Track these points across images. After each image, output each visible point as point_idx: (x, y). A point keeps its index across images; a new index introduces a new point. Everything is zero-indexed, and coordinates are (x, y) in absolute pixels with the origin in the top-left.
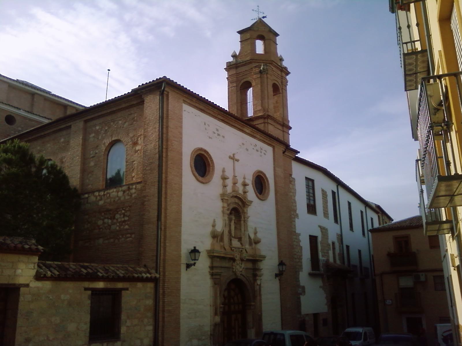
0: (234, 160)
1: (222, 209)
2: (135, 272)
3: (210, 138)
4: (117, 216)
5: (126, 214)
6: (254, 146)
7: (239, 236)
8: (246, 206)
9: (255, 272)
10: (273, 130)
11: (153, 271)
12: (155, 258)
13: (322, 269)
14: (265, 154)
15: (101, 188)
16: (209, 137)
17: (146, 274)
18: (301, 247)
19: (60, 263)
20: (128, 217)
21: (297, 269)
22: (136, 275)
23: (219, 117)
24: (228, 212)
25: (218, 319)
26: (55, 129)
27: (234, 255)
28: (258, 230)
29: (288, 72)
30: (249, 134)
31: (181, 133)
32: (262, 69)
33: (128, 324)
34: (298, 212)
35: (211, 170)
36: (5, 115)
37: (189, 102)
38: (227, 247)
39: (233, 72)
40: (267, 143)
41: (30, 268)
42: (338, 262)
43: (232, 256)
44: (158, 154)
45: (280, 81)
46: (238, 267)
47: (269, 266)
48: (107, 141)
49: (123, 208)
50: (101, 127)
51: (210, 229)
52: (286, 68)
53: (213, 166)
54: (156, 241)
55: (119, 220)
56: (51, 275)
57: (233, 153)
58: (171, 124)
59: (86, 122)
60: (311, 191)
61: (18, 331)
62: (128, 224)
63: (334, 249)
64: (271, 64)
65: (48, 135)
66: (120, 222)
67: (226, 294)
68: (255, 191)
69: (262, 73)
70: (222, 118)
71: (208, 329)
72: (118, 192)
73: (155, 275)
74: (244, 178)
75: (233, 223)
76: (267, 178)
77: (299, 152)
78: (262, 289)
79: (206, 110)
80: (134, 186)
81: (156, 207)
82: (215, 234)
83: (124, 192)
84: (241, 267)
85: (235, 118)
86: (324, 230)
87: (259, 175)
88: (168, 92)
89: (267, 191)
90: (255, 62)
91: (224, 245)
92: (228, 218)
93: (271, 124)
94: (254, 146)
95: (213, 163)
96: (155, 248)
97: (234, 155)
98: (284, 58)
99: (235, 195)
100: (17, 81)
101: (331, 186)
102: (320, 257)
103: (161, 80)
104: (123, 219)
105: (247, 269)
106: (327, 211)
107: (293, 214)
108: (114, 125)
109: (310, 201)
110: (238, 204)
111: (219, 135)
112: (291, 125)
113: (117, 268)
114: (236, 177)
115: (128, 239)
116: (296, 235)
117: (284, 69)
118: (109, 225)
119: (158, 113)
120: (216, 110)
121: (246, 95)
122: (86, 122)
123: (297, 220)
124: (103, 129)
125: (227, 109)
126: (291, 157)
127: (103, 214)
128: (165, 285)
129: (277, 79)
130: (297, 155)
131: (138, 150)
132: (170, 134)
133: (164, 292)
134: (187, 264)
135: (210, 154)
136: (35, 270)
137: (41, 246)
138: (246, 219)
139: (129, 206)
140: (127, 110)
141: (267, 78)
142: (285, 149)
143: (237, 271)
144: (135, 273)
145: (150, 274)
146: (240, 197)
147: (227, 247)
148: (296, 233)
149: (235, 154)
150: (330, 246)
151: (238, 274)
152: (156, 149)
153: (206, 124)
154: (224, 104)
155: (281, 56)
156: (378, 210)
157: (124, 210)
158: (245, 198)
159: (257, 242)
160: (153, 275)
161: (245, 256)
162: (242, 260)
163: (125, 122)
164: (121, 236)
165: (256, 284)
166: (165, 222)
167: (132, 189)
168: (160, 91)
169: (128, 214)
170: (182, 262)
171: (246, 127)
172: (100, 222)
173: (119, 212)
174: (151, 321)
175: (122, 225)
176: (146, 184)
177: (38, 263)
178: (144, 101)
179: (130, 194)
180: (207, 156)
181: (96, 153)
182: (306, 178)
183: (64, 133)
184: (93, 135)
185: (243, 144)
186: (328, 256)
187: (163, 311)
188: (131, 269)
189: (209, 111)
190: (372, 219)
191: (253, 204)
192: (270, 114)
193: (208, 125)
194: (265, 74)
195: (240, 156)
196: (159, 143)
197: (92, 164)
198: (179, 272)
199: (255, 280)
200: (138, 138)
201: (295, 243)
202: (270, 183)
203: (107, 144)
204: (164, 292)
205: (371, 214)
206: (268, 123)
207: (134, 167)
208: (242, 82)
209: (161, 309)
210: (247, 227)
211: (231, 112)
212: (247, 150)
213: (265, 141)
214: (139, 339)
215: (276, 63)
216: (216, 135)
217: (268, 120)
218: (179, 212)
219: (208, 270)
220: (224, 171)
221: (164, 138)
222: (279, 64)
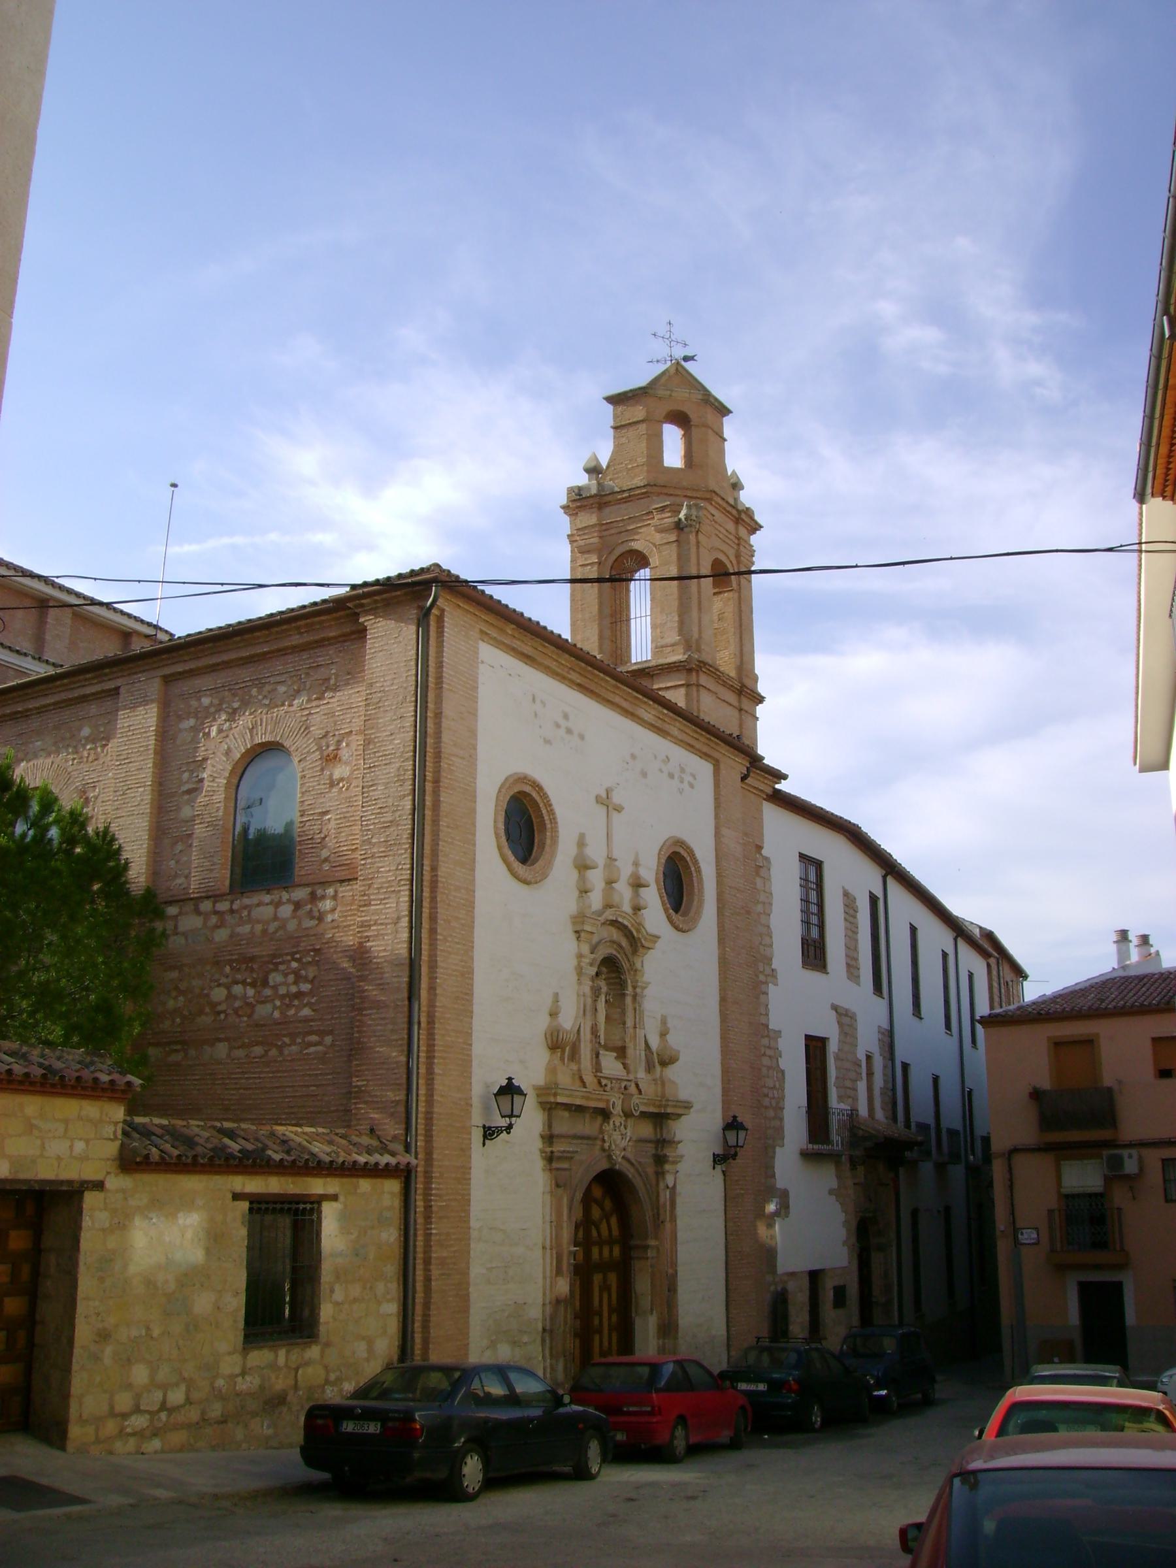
1: (574, 962)
4: (275, 978)
5: (303, 972)
7: (619, 1044)
9: (661, 1151)
10: (715, 709)
11: (400, 1148)
12: (402, 1109)
13: (835, 1137)
14: (692, 786)
18: (783, 1072)
20: (312, 982)
21: (772, 1137)
23: (574, 676)
24: (593, 971)
25: (563, 1286)
26: (63, 696)
27: (608, 1101)
28: (671, 1023)
29: (756, 523)
30: (652, 725)
31: (473, 733)
32: (682, 515)
33: (338, 1295)
34: (775, 964)
35: (548, 841)
38: (589, 1079)
39: (589, 519)
41: (106, 1136)
42: (880, 1115)
43: (601, 1105)
45: (731, 553)
46: (616, 1136)
47: (696, 1135)
52: (748, 512)
53: (555, 830)
55: (282, 990)
56: (162, 1158)
58: (450, 708)
59: (168, 680)
60: (813, 896)
61: (81, 1309)
62: (309, 1004)
63: (870, 1074)
64: (709, 500)
66: (283, 997)
68: (663, 904)
69: (682, 529)
71: (535, 1313)
72: (278, 904)
73: (404, 1159)
74: (636, 864)
75: (601, 1005)
76: (696, 862)
77: (785, 777)
78: (679, 1200)
79: (539, 659)
80: (330, 891)
83: (298, 905)
84: (623, 1136)
85: (596, 669)
86: (845, 1018)
87: (675, 853)
88: (443, 611)
90: (659, 494)
91: (579, 1070)
92: (592, 988)
95: (554, 820)
96: (404, 1081)
97: (608, 791)
99: (611, 918)
101: (868, 878)
102: (834, 1101)
104: (294, 989)
106: (856, 960)
108: (260, 697)
109: (809, 929)
110: (620, 946)
112: (762, 688)
115: (312, 1049)
116: (768, 1036)
117: (743, 516)
118: (247, 1004)
119: (414, 672)
120: (567, 656)
125: (566, 635)
126: (762, 791)
127: (228, 969)
128: (431, 1189)
129: (724, 547)
130: (777, 786)
131: (342, 779)
132: (446, 737)
133: (428, 1208)
138: (638, 990)
139: (314, 950)
143: (613, 1147)
145: (393, 1154)
146: (626, 923)
147: (589, 1079)
150: (860, 1066)
151: (618, 1155)
152: (404, 781)
153: (538, 701)
155: (734, 472)
156: (989, 946)
157: (298, 960)
158: (640, 925)
163: (298, 691)
164: (287, 1040)
165: (662, 1185)
166: (432, 1005)
167: (323, 897)
168: (421, 608)
172: (219, 994)
173: (282, 967)
174: (394, 1288)
175: (289, 1006)
182: (803, 857)
183: (93, 709)
184: (192, 722)
185: (633, 757)
186: (855, 1099)
187: (427, 1262)
189: (547, 662)
190: (971, 976)
191: (659, 944)
193: (542, 702)
196: (415, 765)
198: (465, 1151)
199: (660, 1174)
200: (339, 742)
201: (766, 1061)
203: (239, 756)
204: (428, 1208)
205: (971, 962)
206: (698, 685)
207: (325, 832)
208: (617, 552)
209: (420, 1255)
210: (642, 1012)
211: (579, 646)
212: (644, 774)
213: (692, 746)
214: (363, 1338)
216: (562, 732)
218: (467, 974)
219: (539, 1144)
220: (581, 843)
221: (428, 749)
222: (732, 502)
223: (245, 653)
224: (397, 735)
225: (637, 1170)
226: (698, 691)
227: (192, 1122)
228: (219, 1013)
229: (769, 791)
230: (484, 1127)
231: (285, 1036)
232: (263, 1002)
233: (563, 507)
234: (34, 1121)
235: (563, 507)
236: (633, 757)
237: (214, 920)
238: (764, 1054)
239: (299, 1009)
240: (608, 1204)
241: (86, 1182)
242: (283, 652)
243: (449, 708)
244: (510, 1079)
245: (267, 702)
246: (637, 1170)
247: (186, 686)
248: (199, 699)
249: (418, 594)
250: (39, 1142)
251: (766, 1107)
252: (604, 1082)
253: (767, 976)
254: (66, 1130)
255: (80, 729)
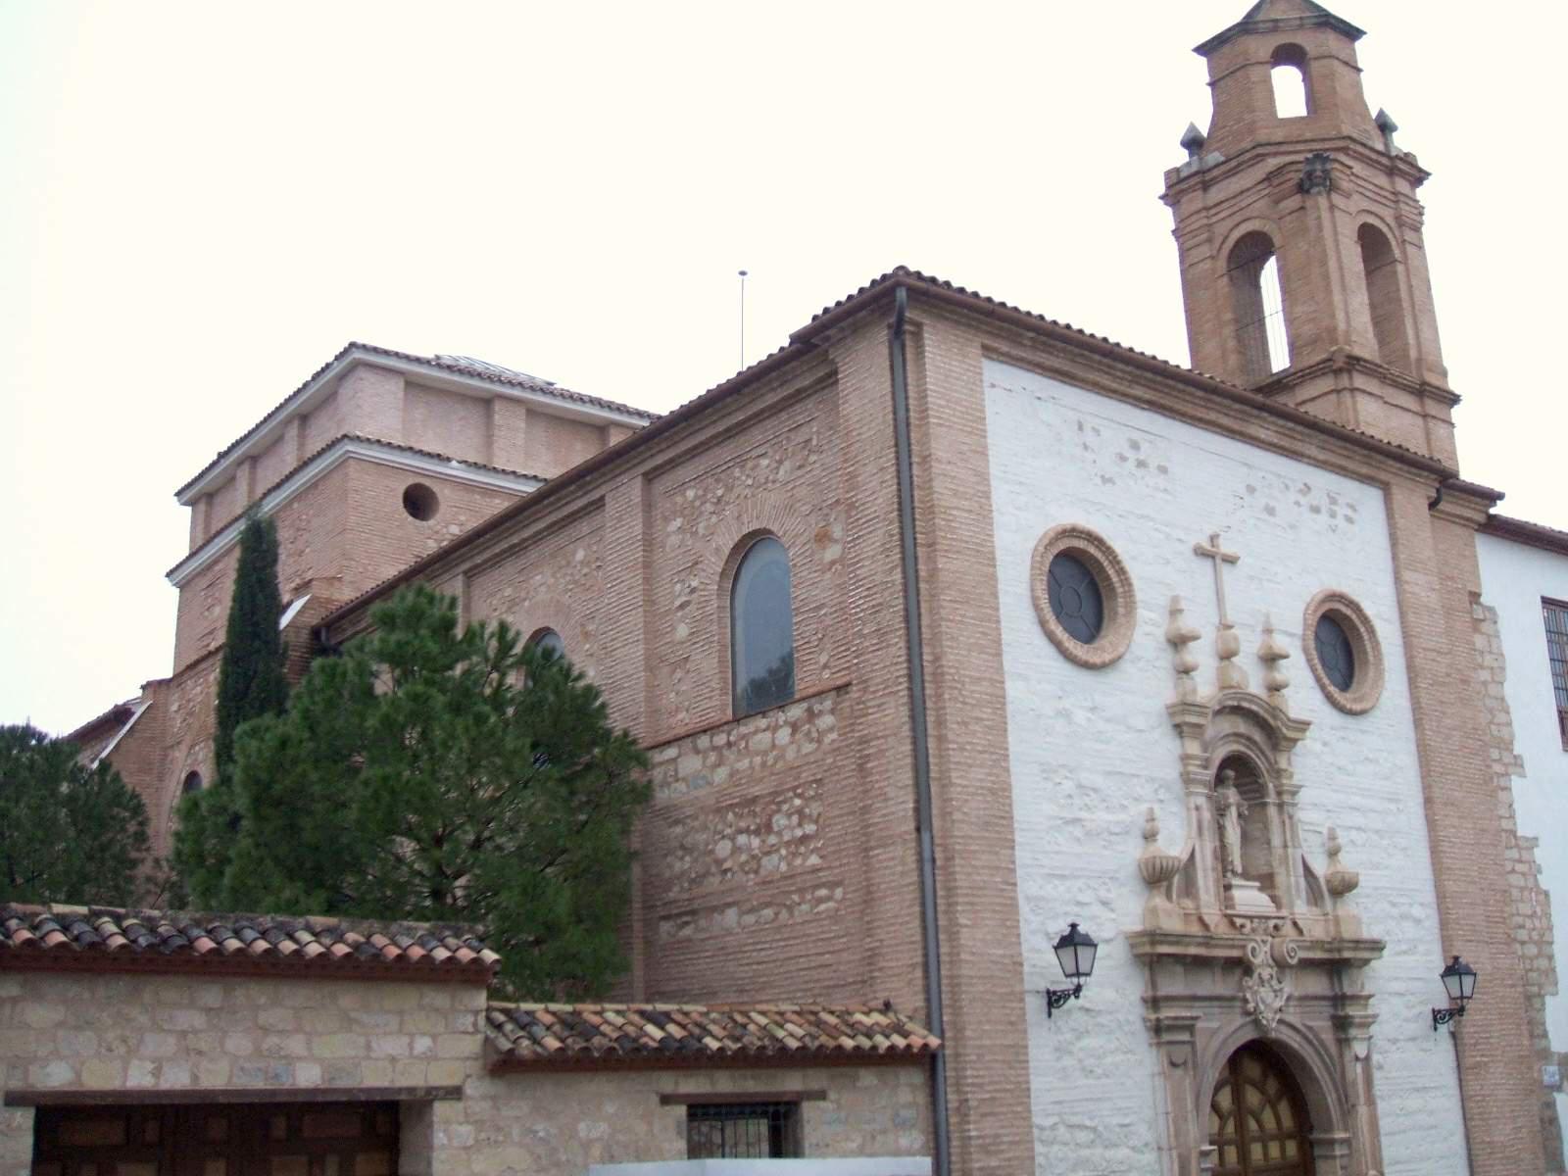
0: (1218, 561)
2: (849, 1031)
3: (1106, 480)
4: (780, 821)
6: (1301, 491)
7: (1264, 870)
8: (1284, 743)
10: (1377, 415)
12: (919, 973)
14: (1350, 520)
15: (715, 717)
16: (1102, 477)
17: (887, 1037)
18: (1546, 894)
19: (569, 1008)
20: (816, 822)
22: (848, 1043)
23: (1138, 391)
26: (553, 518)
27: (1244, 947)
28: (1342, 839)
29: (1420, 170)
31: (983, 477)
34: (1517, 750)
35: (1121, 610)
36: (401, 489)
37: (1005, 348)
38: (1212, 914)
40: (1354, 472)
43: (1235, 953)
44: (899, 570)
45: (1388, 214)
46: (1265, 993)
47: (1401, 984)
48: (727, 541)
49: (794, 789)
50: (700, 492)
51: (1133, 852)
52: (1408, 159)
54: (917, 909)
55: (786, 838)
57: (1210, 532)
59: (650, 477)
64: (1344, 150)
65: (537, 538)
66: (788, 844)
67: (1225, 1099)
70: (1148, 395)
72: (775, 729)
76: (1366, 620)
77: (1501, 496)
78: (1377, 1075)
81: (906, 777)
82: (1158, 866)
85: (1222, 396)
88: (919, 325)
89: (1371, 674)
91: (1198, 908)
93: (1370, 394)
94: (1301, 491)
97: (1213, 538)
98: (1394, 117)
100: (438, 363)
103: (888, 283)
104: (799, 833)
105: (1304, 998)
107: (1499, 761)
110: (1249, 739)
111: (1141, 464)
113: (778, 1018)
114: (1230, 627)
115: (822, 907)
117: (1402, 166)
118: (754, 857)
121: (1257, 287)
122: (650, 477)
123: (1516, 782)
124: (709, 496)
125: (1179, 356)
127: (730, 816)
130: (1492, 511)
134: (1048, 992)
135: (1109, 548)
136: (480, 1037)
137: (491, 949)
138: (1286, 798)
139: (815, 781)
140: (784, 416)
141: (1332, 207)
142: (1438, 490)
143: (1262, 1007)
144: (849, 1036)
145: (905, 1035)
146: (1254, 708)
147: (1212, 914)
148: (1515, 837)
149: (1218, 536)
151: (1269, 1018)
153: (1087, 427)
154: (1168, 342)
157: (799, 796)
158: (1275, 711)
159: (1342, 888)
160: (917, 1041)
161: (1293, 949)
162: (1281, 965)
163: (780, 462)
165: (1348, 1057)
168: (889, 327)
169: (814, 809)
170: (1027, 986)
171: (1257, 417)
172: (723, 848)
173: (785, 807)
175: (795, 855)
176: (865, 690)
177: (489, 1009)
178: (835, 372)
179: (815, 735)
180: (1099, 555)
181: (693, 591)
182: (1547, 602)
183: (584, 527)
184: (678, 522)
185: (1251, 489)
188: (832, 1020)
189: (1092, 376)
192: (1357, 352)
194: (1319, 193)
195: (1246, 543)
197: (682, 631)
198: (1017, 1025)
199: (1343, 1042)
202: (1380, 639)
206: (1353, 390)
212: (1270, 511)
215: (1364, 145)
216: (1131, 465)
217: (1351, 378)
218: (1000, 792)
222: (1380, 147)
223: (721, 427)
224: (879, 494)
225: (1306, 1038)
226: (1353, 397)
227: (607, 1006)
228: (726, 871)
229: (1481, 518)
230: (1048, 992)
231: (792, 892)
232: (768, 853)
233: (1162, 198)
234: (353, 1015)
235: (1162, 198)
236: (1251, 489)
237: (713, 757)
238: (1513, 871)
239: (805, 857)
240: (1272, 1086)
241: (437, 1088)
242: (758, 418)
243: (940, 448)
244: (1074, 926)
245: (750, 482)
246: (1306, 1038)
247: (660, 486)
248: (683, 494)
249: (900, 309)
250: (362, 1040)
251: (1523, 943)
252: (1239, 921)
253: (1506, 765)
254: (401, 1023)
255: (574, 553)
